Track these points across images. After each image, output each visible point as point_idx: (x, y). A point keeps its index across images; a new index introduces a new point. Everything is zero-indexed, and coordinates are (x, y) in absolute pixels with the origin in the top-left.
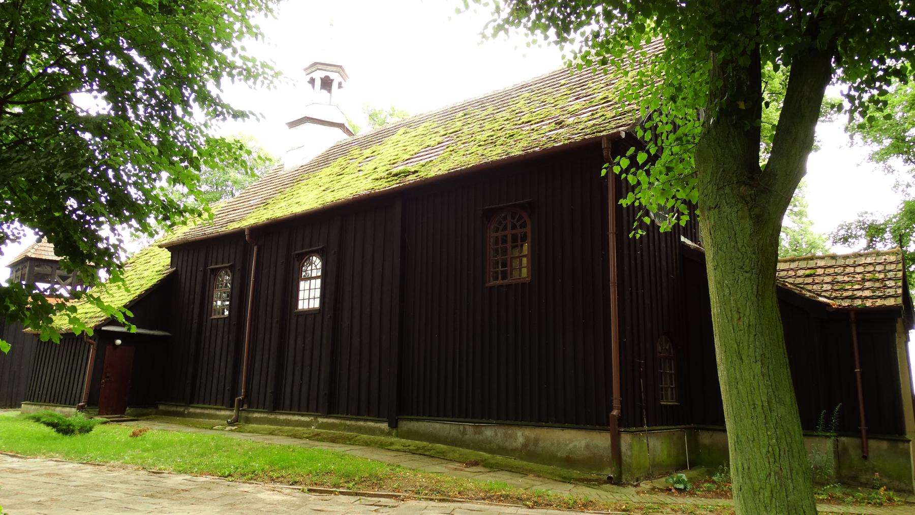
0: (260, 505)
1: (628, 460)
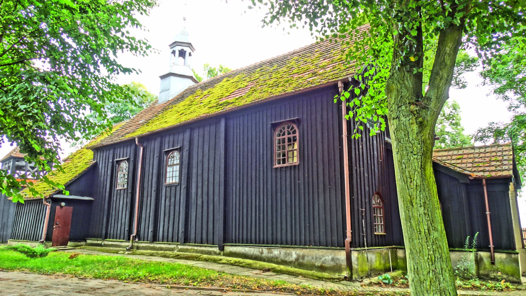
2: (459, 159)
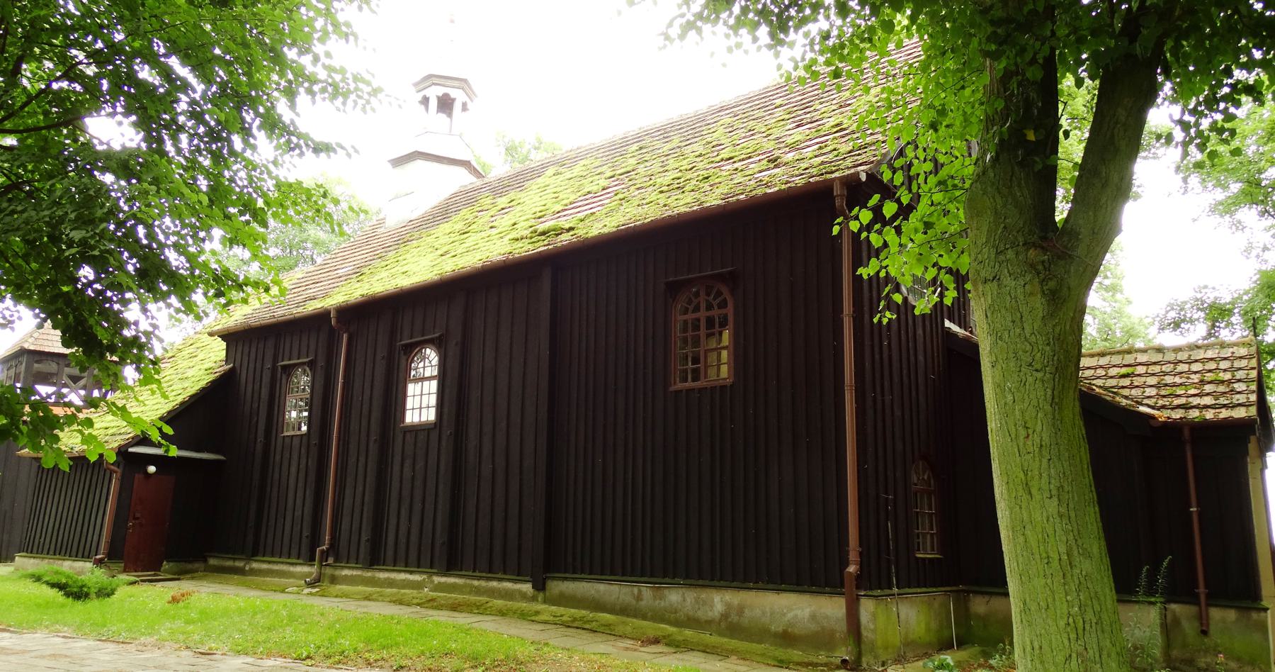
1: (870, 635)
2: (1124, 376)
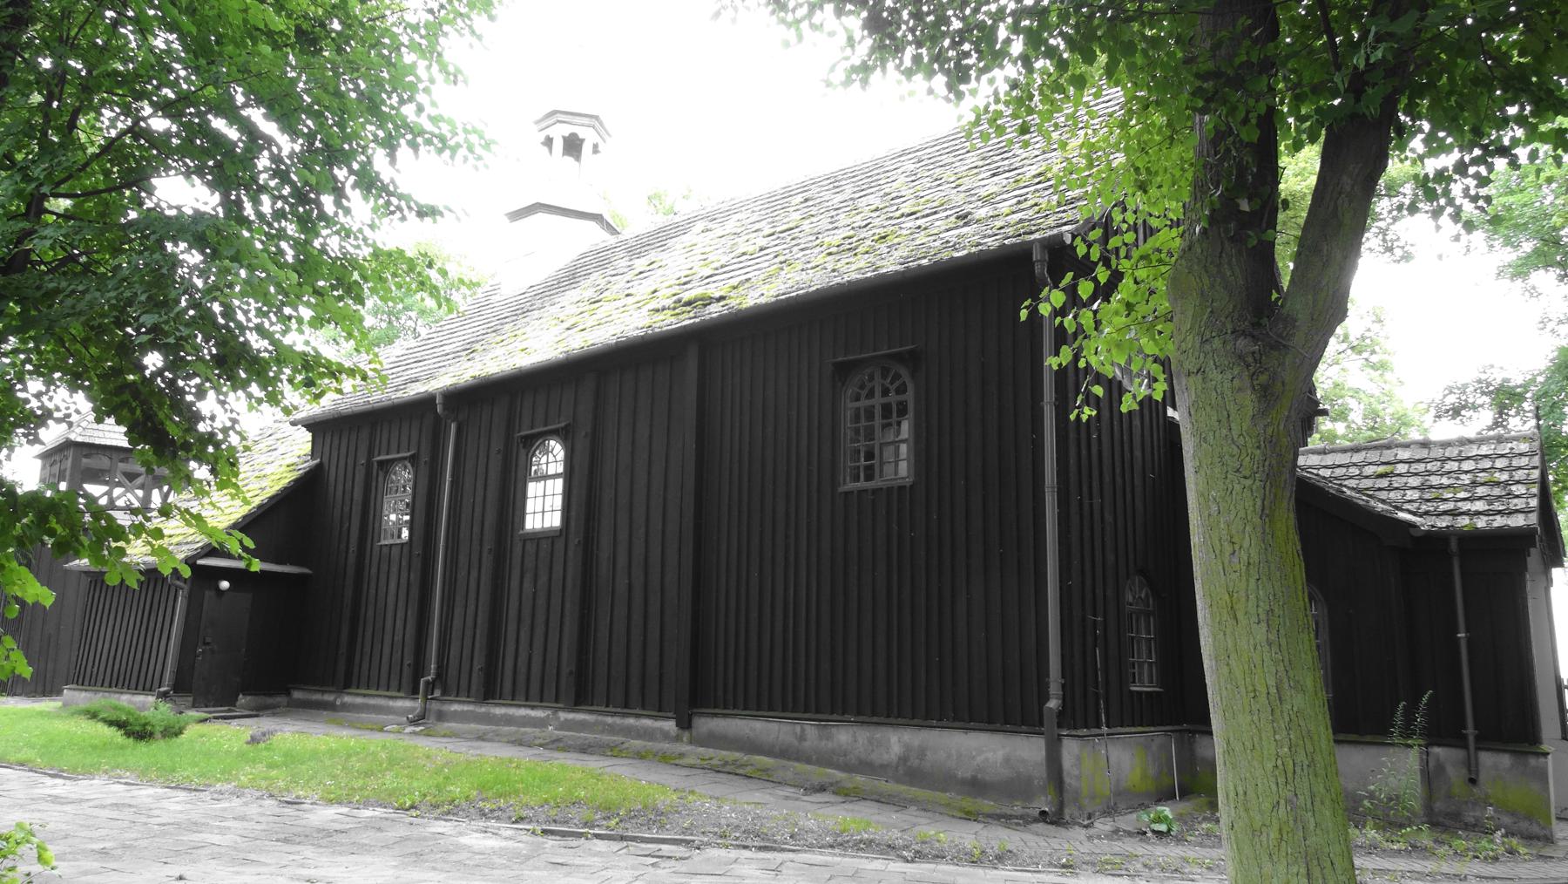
0: (463, 856)
1: (1073, 782)
2: (1381, 476)
